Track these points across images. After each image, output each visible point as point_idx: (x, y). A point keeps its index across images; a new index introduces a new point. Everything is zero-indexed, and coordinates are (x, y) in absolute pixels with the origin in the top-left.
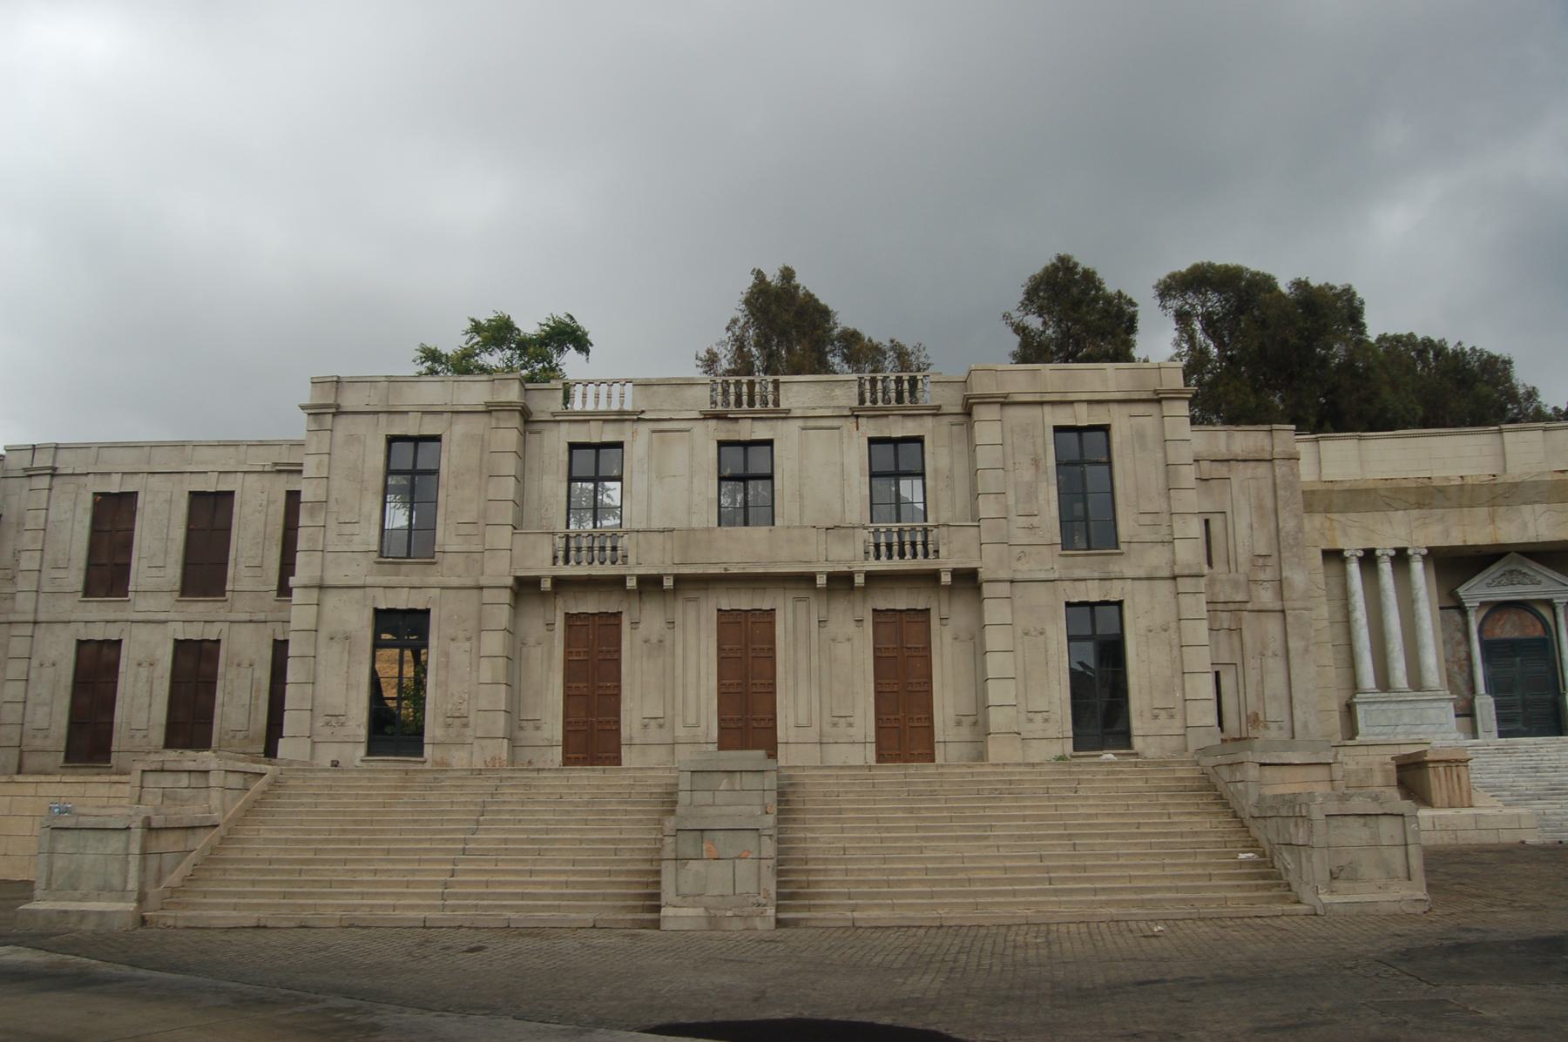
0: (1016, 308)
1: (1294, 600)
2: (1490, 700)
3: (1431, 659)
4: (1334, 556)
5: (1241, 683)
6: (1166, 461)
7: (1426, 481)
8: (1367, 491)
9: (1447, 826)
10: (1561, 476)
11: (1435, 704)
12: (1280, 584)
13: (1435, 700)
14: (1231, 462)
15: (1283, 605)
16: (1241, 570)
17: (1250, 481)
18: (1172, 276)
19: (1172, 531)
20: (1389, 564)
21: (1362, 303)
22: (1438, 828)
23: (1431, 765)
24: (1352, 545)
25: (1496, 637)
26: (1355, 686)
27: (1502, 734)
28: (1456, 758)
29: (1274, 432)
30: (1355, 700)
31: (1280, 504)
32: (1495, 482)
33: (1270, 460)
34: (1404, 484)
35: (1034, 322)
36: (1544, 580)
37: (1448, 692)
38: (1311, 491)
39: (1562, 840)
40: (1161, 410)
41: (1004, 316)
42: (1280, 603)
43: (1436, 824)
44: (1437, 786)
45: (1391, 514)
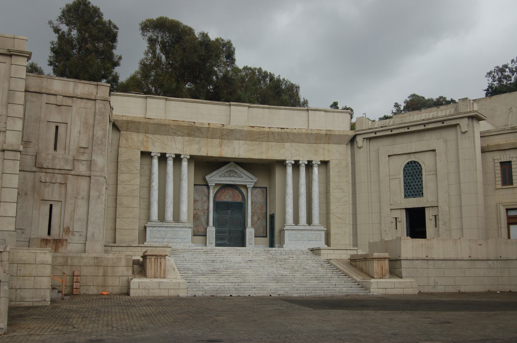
0: (56, 20)
1: (96, 172)
2: (214, 229)
3: (184, 208)
4: (146, 155)
5: (63, 212)
6: (9, 88)
7: (193, 124)
8: (165, 125)
9: (145, 287)
10: (252, 129)
11: (183, 229)
12: (90, 163)
13: (183, 227)
14: (74, 98)
15: (90, 173)
16: (71, 153)
17: (83, 109)
18: (148, 21)
19: (6, 126)
20: (172, 162)
21: (234, 49)
22: (141, 288)
23: (148, 257)
24: (156, 150)
25: (221, 200)
26: (149, 219)
27: (217, 245)
28: (160, 254)
29: (98, 85)
30: (284, 228)
31: (96, 122)
32: (224, 128)
33: (95, 100)
34: (183, 124)
35: (64, 28)
36: (244, 176)
37: (323, 227)
38: (139, 122)
39: (196, 295)
40: (11, 61)
41: (49, 22)
42: (89, 172)
43: (140, 286)
44: (150, 267)
45: (176, 137)
